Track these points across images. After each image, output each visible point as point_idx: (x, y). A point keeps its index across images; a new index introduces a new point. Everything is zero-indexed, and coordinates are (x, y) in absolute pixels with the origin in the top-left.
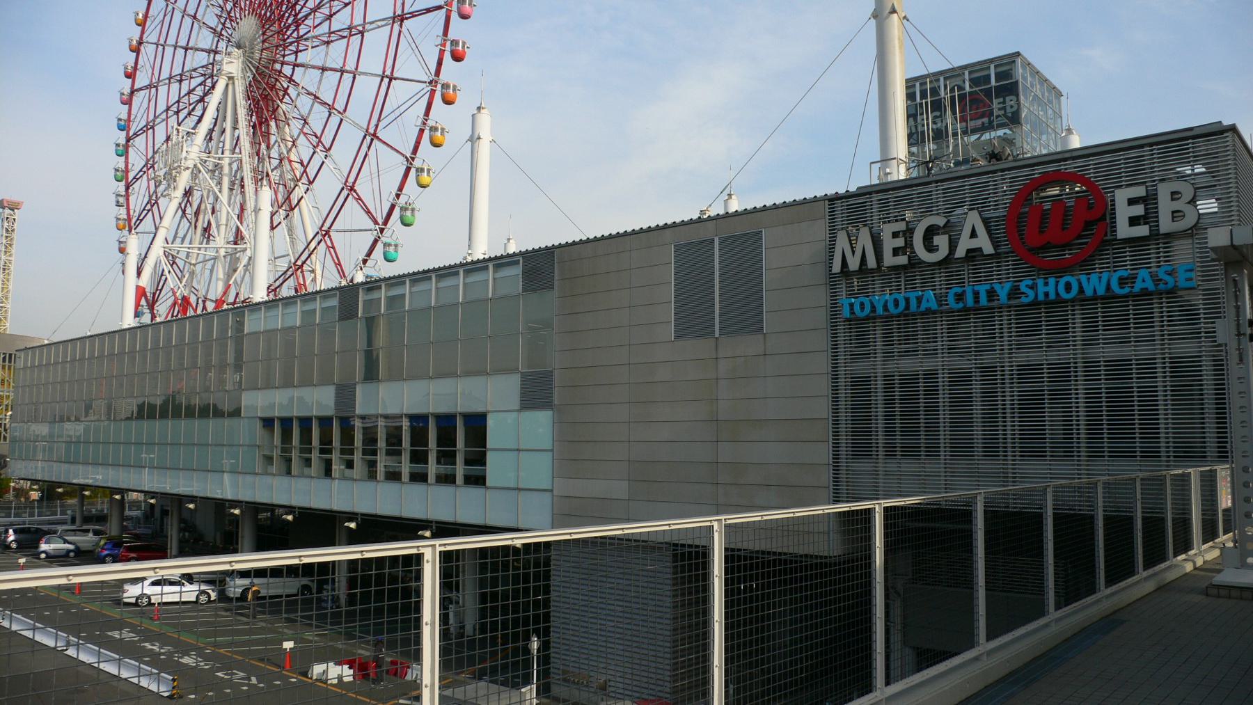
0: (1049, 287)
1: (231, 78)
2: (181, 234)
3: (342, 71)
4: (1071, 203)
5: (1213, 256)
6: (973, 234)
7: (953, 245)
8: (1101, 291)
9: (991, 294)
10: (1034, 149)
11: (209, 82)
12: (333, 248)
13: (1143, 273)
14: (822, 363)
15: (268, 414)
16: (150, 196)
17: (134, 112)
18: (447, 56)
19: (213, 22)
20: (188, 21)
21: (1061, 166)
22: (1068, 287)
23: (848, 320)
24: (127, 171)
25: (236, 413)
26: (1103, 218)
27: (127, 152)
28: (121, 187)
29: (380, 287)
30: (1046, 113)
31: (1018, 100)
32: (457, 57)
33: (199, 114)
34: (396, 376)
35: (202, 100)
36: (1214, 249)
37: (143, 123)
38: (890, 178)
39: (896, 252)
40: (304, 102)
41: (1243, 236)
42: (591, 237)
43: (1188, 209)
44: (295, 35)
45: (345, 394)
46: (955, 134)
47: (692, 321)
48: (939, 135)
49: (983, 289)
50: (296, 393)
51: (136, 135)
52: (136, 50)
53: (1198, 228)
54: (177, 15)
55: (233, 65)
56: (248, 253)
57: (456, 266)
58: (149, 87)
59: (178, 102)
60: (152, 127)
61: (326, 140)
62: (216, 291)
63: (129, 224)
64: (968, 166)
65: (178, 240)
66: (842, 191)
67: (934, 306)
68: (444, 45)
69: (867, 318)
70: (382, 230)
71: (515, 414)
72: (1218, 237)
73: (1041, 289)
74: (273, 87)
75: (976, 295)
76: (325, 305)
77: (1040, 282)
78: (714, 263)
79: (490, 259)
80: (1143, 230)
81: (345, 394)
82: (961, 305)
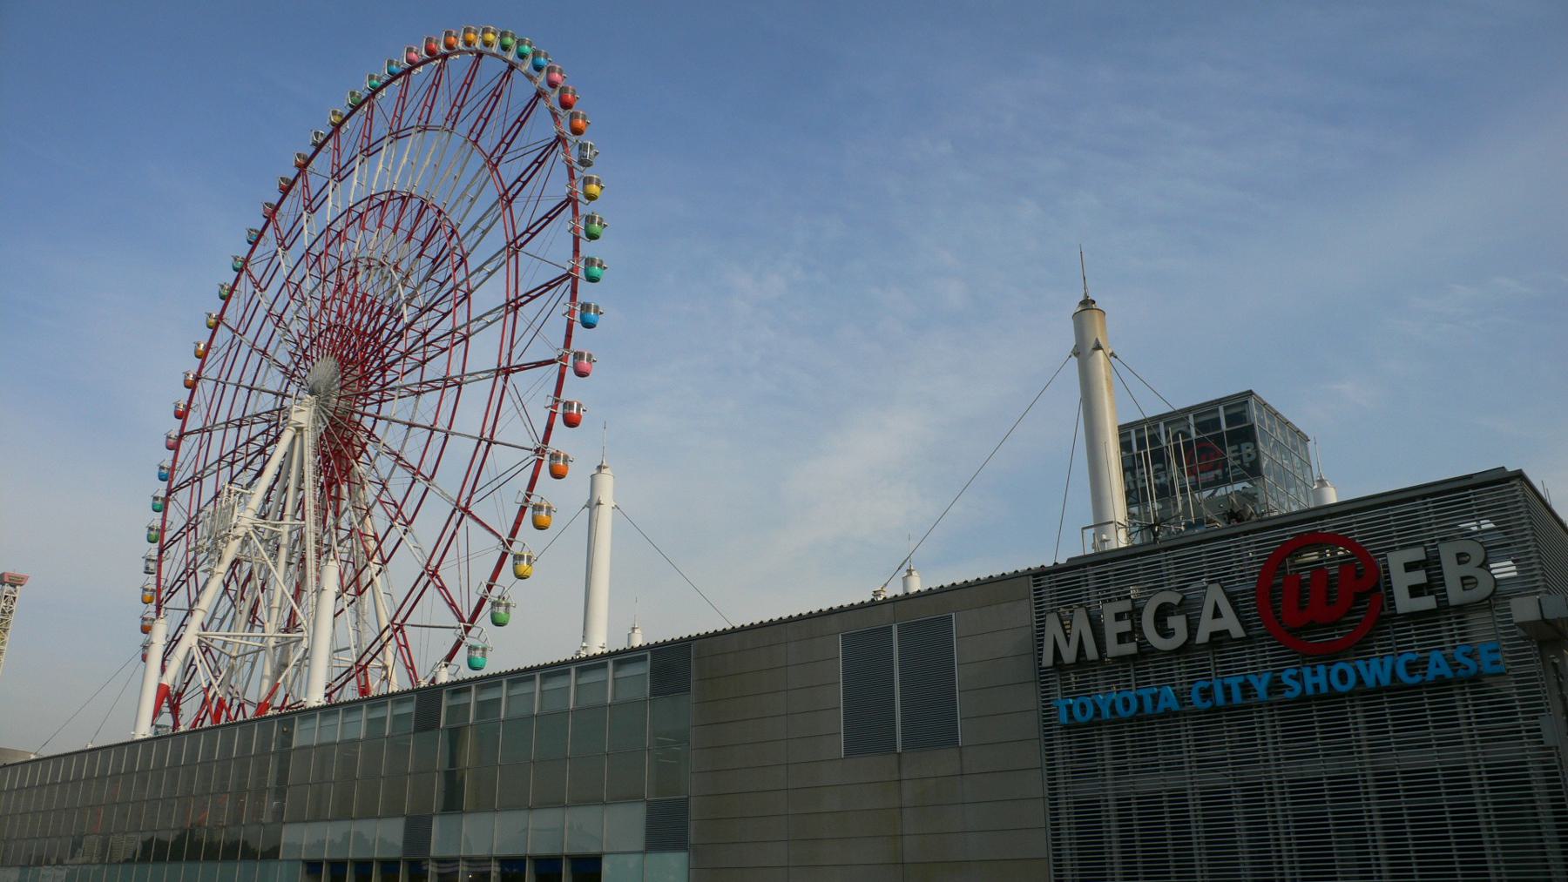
0: (1318, 678)
1: (299, 429)
2: (220, 615)
3: (432, 429)
4: (1334, 570)
5: (1522, 633)
6: (1217, 614)
7: (1192, 628)
8: (1385, 681)
9: (1246, 688)
10: (1281, 505)
11: (273, 431)
12: (406, 646)
13: (1436, 656)
14: (1036, 785)
15: (315, 856)
16: (188, 565)
17: (180, 459)
18: (559, 419)
19: (284, 359)
20: (256, 356)
21: (1317, 526)
22: (1343, 676)
23: (1066, 727)
24: (163, 530)
25: (272, 854)
26: (1377, 588)
27: (166, 508)
28: (153, 550)
29: (469, 690)
30: (1291, 461)
31: (1256, 447)
32: (571, 422)
33: (258, 467)
34: (485, 805)
35: (262, 451)
36: (1522, 625)
37: (189, 474)
38: (1108, 547)
39: (1121, 638)
40: (385, 464)
41: (1555, 608)
42: (738, 626)
43: (1480, 574)
44: (380, 381)
45: (417, 831)
46: (1183, 490)
47: (867, 734)
48: (1164, 492)
49: (1235, 682)
50: (354, 827)
51: (179, 487)
52: (192, 386)
53: (1498, 596)
54: (245, 349)
55: (303, 414)
56: (305, 644)
57: (566, 662)
58: (202, 431)
59: (234, 452)
60: (200, 480)
61: (408, 511)
62: (257, 690)
63: (157, 599)
64: (1203, 529)
65: (216, 622)
66: (1049, 564)
67: (1175, 707)
68: (555, 407)
69: (1091, 723)
70: (467, 629)
71: (638, 857)
72: (1524, 610)
73: (1309, 681)
74: (349, 443)
75: (1227, 690)
76: (397, 712)
77: (1307, 671)
78: (892, 658)
79: (610, 654)
80: (1428, 602)
81: (417, 831)
82: (1208, 704)
